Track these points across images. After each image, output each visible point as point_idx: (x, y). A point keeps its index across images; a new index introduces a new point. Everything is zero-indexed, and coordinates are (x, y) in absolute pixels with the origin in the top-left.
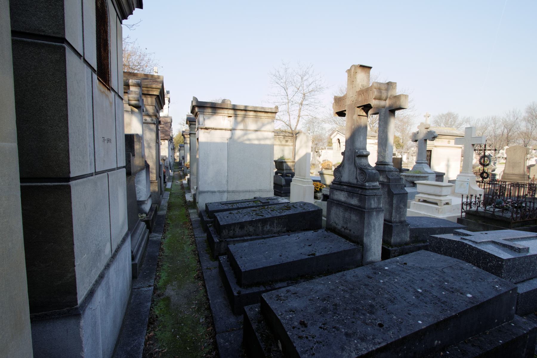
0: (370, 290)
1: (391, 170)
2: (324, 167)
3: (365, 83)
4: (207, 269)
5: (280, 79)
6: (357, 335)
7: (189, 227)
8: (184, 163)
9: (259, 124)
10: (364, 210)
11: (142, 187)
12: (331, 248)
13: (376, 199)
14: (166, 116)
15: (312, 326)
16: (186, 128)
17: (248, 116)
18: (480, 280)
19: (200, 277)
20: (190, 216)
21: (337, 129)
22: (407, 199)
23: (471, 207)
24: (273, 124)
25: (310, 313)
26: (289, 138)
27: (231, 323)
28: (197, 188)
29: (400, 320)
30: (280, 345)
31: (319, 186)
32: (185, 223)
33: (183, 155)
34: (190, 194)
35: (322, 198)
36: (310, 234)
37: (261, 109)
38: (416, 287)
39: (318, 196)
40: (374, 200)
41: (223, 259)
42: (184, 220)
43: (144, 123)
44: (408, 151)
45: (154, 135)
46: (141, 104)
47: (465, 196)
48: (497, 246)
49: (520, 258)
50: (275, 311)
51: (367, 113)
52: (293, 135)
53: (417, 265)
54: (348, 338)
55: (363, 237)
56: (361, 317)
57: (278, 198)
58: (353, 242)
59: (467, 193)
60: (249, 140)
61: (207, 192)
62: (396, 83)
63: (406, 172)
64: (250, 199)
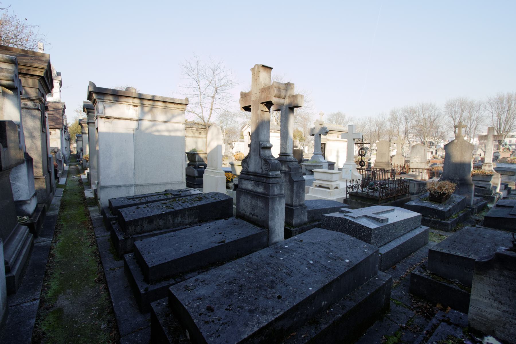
0: (271, 268)
1: (291, 161)
2: (236, 158)
3: (267, 82)
4: (111, 269)
5: (192, 71)
6: (259, 310)
7: (88, 227)
8: (83, 155)
9: (169, 115)
10: (268, 197)
11: (22, 185)
12: (240, 234)
13: (278, 187)
14: (57, 101)
15: (218, 309)
16: (83, 116)
17: (157, 107)
18: (355, 247)
19: (102, 280)
20: (90, 214)
21: (248, 123)
22: (305, 186)
23: (353, 190)
24: (183, 116)
25: (217, 297)
26: (202, 130)
27: (138, 323)
28: (98, 183)
29: (295, 290)
30: (188, 334)
31: (230, 177)
32: (83, 223)
33: (81, 147)
34: (90, 190)
35: (233, 188)
36: (221, 223)
37: (170, 99)
38: (309, 260)
39: (230, 186)
40: (277, 187)
41: (129, 257)
42: (83, 220)
43: (23, 108)
44: (309, 144)
45: (38, 124)
46: (16, 85)
47: (348, 181)
48: (368, 219)
49: (382, 227)
50: (182, 302)
51: (269, 109)
52: (206, 127)
53: (310, 241)
54: (251, 314)
55: (268, 221)
56: (263, 293)
57: (190, 189)
58: (260, 226)
59: (351, 179)
60: (158, 131)
61: (111, 187)
62: (294, 84)
63: (306, 162)
64: (161, 192)
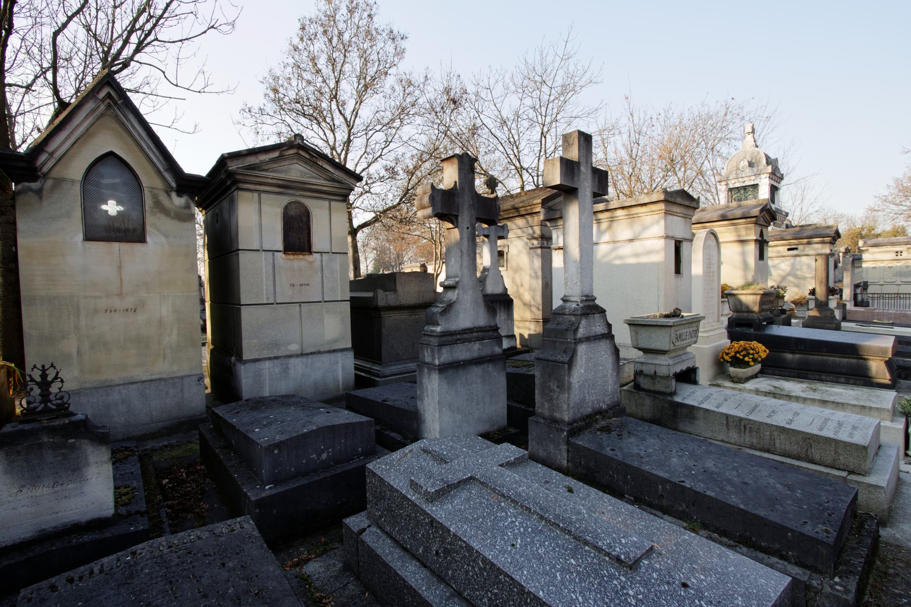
9: (637, 227)
17: (616, 219)
60: (621, 258)
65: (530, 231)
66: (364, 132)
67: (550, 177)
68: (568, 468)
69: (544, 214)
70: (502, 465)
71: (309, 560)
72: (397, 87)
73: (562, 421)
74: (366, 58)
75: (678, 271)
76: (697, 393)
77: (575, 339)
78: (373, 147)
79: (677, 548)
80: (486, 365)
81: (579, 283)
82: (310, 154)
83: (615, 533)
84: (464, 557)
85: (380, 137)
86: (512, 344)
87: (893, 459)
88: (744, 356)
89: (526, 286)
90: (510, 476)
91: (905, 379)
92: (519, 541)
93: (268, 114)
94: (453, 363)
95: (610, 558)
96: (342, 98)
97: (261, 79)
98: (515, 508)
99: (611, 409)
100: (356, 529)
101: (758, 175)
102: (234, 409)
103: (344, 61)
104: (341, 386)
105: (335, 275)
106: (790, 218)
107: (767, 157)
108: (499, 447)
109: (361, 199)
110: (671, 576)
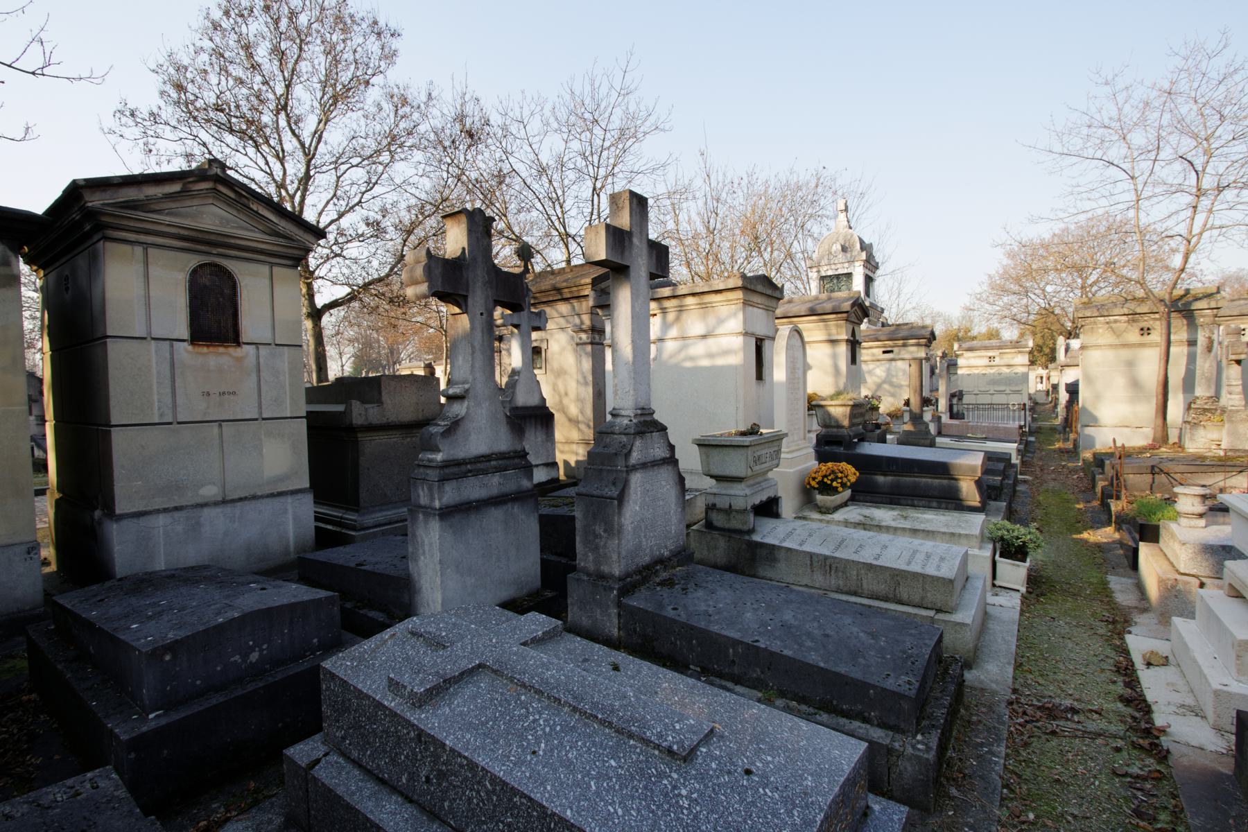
9: (712, 320)
26: (1155, 319)
60: (692, 358)
65: (577, 321)
66: (333, 166)
67: (593, 249)
68: (619, 638)
69: (595, 299)
70: (524, 644)
71: (227, 820)
72: (385, 105)
73: (612, 576)
74: (335, 56)
75: (760, 376)
76: (779, 529)
77: (627, 467)
78: (348, 188)
79: (743, 727)
80: (509, 505)
81: (632, 392)
82: (236, 192)
83: (667, 717)
84: (466, 779)
85: (359, 174)
86: (553, 474)
87: (979, 592)
88: (832, 480)
89: (572, 395)
90: (536, 656)
91: (995, 500)
92: (543, 745)
93: (166, 123)
94: (462, 504)
95: (660, 751)
96: (297, 112)
97: (154, 67)
98: (539, 701)
99: (675, 556)
100: (304, 762)
101: (851, 262)
102: (95, 596)
103: (299, 56)
104: (292, 548)
105: (282, 378)
106: (886, 314)
107: (862, 242)
108: (523, 618)
109: (327, 266)
110: (733, 764)
